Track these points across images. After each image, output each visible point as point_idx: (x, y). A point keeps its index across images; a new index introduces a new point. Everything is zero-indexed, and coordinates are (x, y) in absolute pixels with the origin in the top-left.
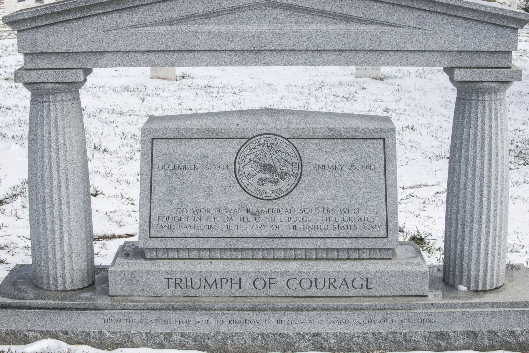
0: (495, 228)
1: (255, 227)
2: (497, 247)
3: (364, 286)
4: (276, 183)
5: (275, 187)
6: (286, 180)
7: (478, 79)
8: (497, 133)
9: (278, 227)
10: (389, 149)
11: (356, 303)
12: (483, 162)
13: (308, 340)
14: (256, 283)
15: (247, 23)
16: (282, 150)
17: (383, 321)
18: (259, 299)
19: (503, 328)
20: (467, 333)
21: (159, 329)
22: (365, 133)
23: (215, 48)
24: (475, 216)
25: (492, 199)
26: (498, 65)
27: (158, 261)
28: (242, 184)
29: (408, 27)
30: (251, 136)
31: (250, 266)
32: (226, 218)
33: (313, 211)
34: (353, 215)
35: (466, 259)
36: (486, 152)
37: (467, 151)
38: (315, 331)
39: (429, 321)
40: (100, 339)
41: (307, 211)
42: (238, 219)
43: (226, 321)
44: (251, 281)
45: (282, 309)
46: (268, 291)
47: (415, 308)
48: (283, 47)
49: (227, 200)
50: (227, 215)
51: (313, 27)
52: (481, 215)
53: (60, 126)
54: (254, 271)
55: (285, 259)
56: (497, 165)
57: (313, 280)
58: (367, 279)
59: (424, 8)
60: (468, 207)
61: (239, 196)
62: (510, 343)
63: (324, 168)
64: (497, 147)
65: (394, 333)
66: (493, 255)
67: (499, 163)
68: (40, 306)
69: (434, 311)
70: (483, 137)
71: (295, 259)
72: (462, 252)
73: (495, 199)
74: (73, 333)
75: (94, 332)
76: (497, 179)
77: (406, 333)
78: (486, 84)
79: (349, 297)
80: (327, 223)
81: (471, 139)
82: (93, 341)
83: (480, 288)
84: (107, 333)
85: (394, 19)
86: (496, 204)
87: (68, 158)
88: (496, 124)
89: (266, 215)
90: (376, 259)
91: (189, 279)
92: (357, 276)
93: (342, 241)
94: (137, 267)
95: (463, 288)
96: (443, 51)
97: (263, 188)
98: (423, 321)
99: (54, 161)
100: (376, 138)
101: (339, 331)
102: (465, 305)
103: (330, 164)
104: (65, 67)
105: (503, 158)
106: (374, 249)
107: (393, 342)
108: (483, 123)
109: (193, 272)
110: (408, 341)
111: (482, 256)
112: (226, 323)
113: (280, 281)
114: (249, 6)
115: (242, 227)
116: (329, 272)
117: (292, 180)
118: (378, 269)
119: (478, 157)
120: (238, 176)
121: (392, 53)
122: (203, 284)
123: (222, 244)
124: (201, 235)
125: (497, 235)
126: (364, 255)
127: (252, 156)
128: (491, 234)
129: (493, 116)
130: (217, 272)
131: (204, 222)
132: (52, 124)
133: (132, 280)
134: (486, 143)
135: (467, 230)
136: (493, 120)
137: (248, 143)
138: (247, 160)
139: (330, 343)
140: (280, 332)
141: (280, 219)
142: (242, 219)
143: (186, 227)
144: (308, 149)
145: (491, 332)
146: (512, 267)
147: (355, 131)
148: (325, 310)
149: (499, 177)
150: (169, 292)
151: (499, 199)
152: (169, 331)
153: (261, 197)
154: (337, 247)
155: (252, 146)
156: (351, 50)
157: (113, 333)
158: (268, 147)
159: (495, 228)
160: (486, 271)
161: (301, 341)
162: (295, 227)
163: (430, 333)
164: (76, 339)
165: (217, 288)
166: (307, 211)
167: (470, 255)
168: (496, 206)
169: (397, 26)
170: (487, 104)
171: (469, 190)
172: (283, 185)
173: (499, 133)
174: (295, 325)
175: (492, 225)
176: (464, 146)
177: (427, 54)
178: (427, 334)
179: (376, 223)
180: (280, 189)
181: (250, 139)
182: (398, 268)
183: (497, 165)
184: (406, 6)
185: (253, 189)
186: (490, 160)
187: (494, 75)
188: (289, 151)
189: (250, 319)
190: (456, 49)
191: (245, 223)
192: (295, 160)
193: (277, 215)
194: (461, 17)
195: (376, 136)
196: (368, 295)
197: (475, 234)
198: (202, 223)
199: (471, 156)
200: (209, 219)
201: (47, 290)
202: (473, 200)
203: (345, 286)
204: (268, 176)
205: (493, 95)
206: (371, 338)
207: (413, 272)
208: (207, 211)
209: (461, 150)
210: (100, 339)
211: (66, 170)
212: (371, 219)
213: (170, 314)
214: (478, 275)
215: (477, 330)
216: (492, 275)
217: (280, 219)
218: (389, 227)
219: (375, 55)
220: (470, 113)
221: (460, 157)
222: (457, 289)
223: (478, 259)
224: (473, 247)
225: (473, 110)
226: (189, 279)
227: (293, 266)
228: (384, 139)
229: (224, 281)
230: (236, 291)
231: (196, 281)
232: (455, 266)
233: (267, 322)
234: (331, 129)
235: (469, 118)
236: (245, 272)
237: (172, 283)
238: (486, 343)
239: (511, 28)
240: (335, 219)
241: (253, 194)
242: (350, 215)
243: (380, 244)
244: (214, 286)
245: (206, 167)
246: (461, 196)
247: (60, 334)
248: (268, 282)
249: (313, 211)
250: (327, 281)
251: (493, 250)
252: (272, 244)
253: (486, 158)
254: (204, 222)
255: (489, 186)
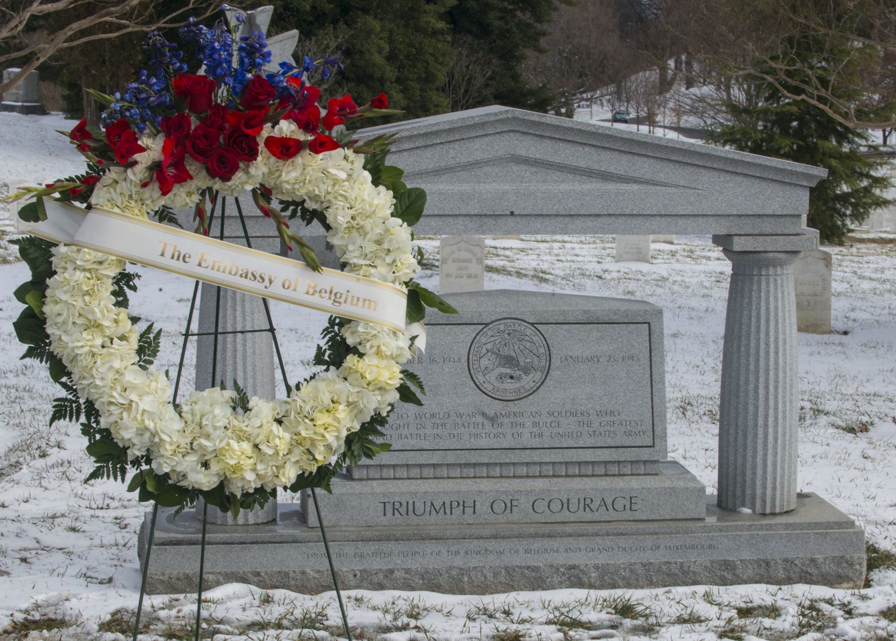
0: (784, 434)
1: (492, 435)
2: (787, 458)
3: (628, 507)
4: (519, 379)
5: (518, 385)
6: (531, 375)
7: (761, 249)
8: (784, 315)
9: (520, 435)
10: (655, 336)
11: (622, 527)
12: (768, 351)
13: (563, 574)
14: (494, 506)
15: (484, 183)
16: (526, 338)
17: (654, 548)
18: (498, 526)
19: (801, 555)
20: (758, 561)
21: (377, 564)
22: (627, 316)
23: (447, 212)
24: (760, 419)
25: (780, 397)
26: (785, 232)
27: (370, 482)
28: (477, 381)
29: (677, 186)
30: (488, 321)
31: (486, 485)
32: (456, 424)
33: (564, 413)
34: (612, 418)
35: (749, 473)
36: (772, 339)
37: (748, 338)
38: (571, 562)
39: (710, 547)
40: (302, 580)
41: (556, 414)
42: (472, 426)
43: (462, 552)
44: (488, 504)
45: (530, 536)
46: (510, 516)
47: (692, 532)
48: (529, 211)
49: (458, 401)
50: (459, 420)
51: (564, 187)
52: (766, 417)
53: (248, 310)
54: (492, 491)
55: (528, 477)
56: (784, 354)
57: (565, 501)
58: (631, 498)
59: (697, 163)
60: (751, 408)
61: (473, 397)
62: (811, 574)
63: (576, 360)
64: (784, 333)
65: (668, 563)
66: (783, 468)
67: (788, 352)
68: (222, 541)
69: (716, 534)
70: (768, 320)
71: (540, 476)
72: (744, 465)
73: (784, 397)
74: (266, 573)
75: (294, 572)
76: (785, 372)
77: (682, 563)
78: (771, 255)
79: (609, 522)
80: (580, 429)
81: (753, 323)
82: (292, 582)
83: (768, 511)
84: (311, 573)
85: (661, 177)
86: (784, 403)
87: (257, 351)
88: (783, 304)
89: (506, 420)
90: (639, 475)
91: (411, 502)
92: (618, 494)
93: (599, 451)
94: (345, 489)
95: (747, 511)
96: (719, 216)
97: (503, 386)
98: (702, 546)
99: (239, 355)
100: (638, 325)
101: (600, 562)
102: (753, 527)
103: (585, 355)
104: (258, 235)
105: (791, 346)
106: (637, 462)
107: (667, 575)
108: (768, 303)
109: (415, 494)
110: (686, 573)
111: (770, 469)
112: (462, 555)
113: (524, 503)
114: (488, 161)
115: (476, 436)
116: (584, 490)
117: (538, 376)
118: (643, 485)
119: (762, 346)
120: (472, 372)
121: (658, 219)
122: (428, 509)
123: (451, 458)
124: (425, 447)
125: (787, 442)
126: (625, 470)
127: (489, 346)
128: (779, 442)
129: (780, 295)
130: (446, 493)
131: (429, 431)
132: (239, 308)
133: (338, 505)
134: (772, 328)
135: (750, 437)
136: (780, 300)
137: (486, 329)
138: (484, 351)
139: (590, 577)
140: (529, 564)
141: (522, 425)
142: (476, 425)
143: (406, 437)
144: (558, 336)
145: (786, 561)
146: (801, 496)
147: (615, 313)
148: (582, 536)
149: (788, 371)
150: (384, 521)
151: (788, 398)
152: (391, 567)
153: (500, 398)
154: (593, 460)
155: (490, 333)
156: (610, 215)
157: (319, 572)
158: (509, 334)
159: (784, 434)
160: (774, 488)
161: (555, 576)
162: (541, 435)
163: (712, 562)
164: (269, 582)
165: (445, 513)
166: (556, 414)
167: (754, 468)
168: (785, 406)
169: (665, 185)
170: (771, 279)
171: (752, 386)
172: (528, 381)
173: (787, 315)
174: (546, 556)
175: (780, 429)
176: (744, 332)
177: (700, 219)
178: (708, 564)
179: (640, 428)
180: (523, 387)
181: (487, 325)
182: (668, 484)
183: (784, 354)
184: (676, 161)
185: (490, 387)
186: (777, 348)
187: (782, 243)
188: (535, 339)
189: (491, 549)
190: (735, 213)
191: (479, 431)
192: (542, 350)
193: (519, 420)
194: (741, 174)
195: (640, 320)
196: (631, 519)
197: (760, 441)
198: (427, 431)
199: (753, 345)
200: (435, 426)
201: (222, 525)
202: (756, 398)
203: (604, 508)
204: (509, 371)
205: (779, 269)
206: (640, 570)
207: (687, 488)
208: (433, 416)
209: (740, 337)
210: (302, 580)
211: (254, 366)
212: (633, 424)
213: (392, 546)
214: (764, 494)
215: (769, 557)
216: (782, 494)
217: (522, 425)
218: (656, 433)
219: (638, 221)
220: (751, 291)
221: (739, 347)
222: (739, 512)
223: (765, 473)
224: (758, 457)
225: (755, 287)
226: (411, 502)
227: (539, 484)
228: (649, 323)
229: (455, 504)
230: (469, 517)
231: (419, 506)
232: (735, 484)
233: (513, 552)
234: (585, 312)
235: (750, 297)
236: (481, 492)
237: (389, 508)
238: (781, 574)
239: (801, 186)
240: (590, 424)
241: (489, 394)
242: (608, 418)
243: (645, 454)
244: (442, 511)
245: (433, 361)
246: (742, 394)
247: (250, 575)
248: (509, 505)
249: (564, 413)
250: (582, 502)
251: (783, 461)
252: (513, 457)
253: (772, 346)
254: (429, 431)
255: (776, 382)
